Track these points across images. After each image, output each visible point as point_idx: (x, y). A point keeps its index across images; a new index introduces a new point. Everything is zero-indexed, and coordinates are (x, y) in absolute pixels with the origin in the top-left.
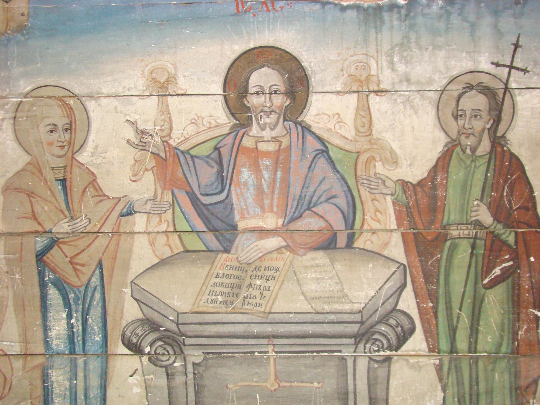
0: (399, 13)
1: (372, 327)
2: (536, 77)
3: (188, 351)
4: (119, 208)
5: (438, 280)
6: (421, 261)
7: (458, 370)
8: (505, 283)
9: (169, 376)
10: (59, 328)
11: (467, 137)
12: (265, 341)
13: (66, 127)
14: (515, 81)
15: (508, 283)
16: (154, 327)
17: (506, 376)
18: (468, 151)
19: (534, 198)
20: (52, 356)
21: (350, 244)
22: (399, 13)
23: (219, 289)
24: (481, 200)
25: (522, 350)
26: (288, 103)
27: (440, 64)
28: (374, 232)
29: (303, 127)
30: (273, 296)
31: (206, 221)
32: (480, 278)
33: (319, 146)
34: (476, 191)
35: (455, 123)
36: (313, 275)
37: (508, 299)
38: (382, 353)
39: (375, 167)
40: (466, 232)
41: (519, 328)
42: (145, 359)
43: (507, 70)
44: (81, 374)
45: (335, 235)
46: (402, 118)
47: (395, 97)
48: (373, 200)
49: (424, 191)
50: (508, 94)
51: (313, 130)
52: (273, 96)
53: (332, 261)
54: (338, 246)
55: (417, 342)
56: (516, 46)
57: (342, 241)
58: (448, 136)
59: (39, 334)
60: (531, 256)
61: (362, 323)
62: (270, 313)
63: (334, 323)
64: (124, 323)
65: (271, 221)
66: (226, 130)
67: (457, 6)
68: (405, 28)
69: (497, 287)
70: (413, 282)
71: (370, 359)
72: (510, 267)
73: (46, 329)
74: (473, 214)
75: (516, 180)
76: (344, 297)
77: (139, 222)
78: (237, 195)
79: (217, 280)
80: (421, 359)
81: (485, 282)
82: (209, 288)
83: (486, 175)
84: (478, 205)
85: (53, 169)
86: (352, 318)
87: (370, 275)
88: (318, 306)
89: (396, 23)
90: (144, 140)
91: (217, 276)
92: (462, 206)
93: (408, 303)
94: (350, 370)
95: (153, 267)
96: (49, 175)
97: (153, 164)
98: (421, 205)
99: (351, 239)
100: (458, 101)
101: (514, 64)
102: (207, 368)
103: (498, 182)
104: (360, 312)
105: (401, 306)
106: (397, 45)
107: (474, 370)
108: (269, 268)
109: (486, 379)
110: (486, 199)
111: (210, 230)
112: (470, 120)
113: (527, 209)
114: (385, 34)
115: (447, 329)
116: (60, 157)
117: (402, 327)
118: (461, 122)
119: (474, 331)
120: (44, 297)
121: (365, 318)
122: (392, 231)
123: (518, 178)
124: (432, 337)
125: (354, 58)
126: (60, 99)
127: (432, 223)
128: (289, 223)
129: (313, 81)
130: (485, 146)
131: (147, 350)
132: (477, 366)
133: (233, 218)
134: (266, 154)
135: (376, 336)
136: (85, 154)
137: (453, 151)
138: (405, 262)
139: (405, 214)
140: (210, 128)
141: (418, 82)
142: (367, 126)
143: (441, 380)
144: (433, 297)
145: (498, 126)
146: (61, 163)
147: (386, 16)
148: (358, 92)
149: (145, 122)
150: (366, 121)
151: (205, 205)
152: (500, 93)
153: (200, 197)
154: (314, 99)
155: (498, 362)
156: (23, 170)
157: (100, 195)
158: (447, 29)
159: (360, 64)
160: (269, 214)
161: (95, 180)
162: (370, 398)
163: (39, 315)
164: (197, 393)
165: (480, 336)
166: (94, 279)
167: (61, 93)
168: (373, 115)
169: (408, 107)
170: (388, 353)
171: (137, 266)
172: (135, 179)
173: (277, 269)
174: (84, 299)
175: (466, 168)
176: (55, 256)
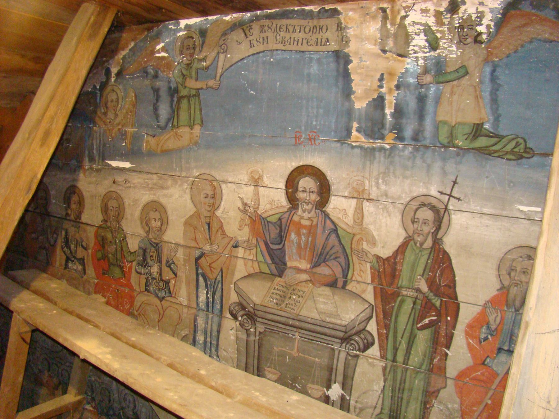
0: (385, 153)
1: (351, 336)
2: (465, 204)
3: (258, 325)
4: (232, 243)
5: (391, 318)
6: (383, 305)
7: (395, 372)
8: (430, 329)
9: (248, 335)
10: (202, 298)
11: (418, 236)
12: (295, 329)
13: (212, 196)
14: (452, 205)
15: (432, 330)
16: (243, 308)
17: (422, 383)
18: (418, 245)
19: (455, 281)
20: (199, 310)
21: (344, 287)
22: (385, 153)
23: (275, 296)
24: (423, 276)
25: (435, 370)
26: (318, 199)
27: (406, 188)
28: (358, 282)
29: (325, 214)
30: (301, 306)
31: (272, 258)
32: (415, 323)
33: (333, 227)
34: (420, 270)
35: (412, 226)
36: (323, 300)
37: (431, 339)
38: (355, 352)
39: (362, 244)
40: (411, 294)
41: (435, 357)
42: (238, 323)
43: (447, 197)
44: (210, 323)
45: (336, 280)
46: (381, 218)
47: (378, 204)
48: (359, 263)
49: (389, 264)
50: (446, 213)
51: (331, 217)
52: (311, 194)
53: (334, 294)
54: (338, 286)
55: (374, 351)
56: (455, 183)
57: (340, 283)
58: (407, 233)
59: (195, 299)
60: (448, 316)
61: (346, 332)
62: (298, 315)
63: (331, 328)
64: (230, 303)
66: (286, 210)
67: (421, 153)
69: (425, 330)
70: (377, 316)
71: (348, 353)
72: (435, 320)
73: (197, 296)
74: (417, 283)
75: (445, 267)
76: (337, 316)
77: (240, 252)
78: (288, 246)
79: (274, 291)
80: (375, 361)
81: (419, 326)
82: (270, 294)
83: (427, 262)
84: (420, 279)
85: (205, 217)
86: (341, 328)
87: (353, 307)
88: (323, 317)
89: (382, 159)
90: (246, 209)
91: (274, 289)
92: (410, 277)
93: (372, 327)
94: (336, 356)
95: (245, 277)
96: (203, 220)
97: (249, 222)
98: (387, 271)
99: (345, 284)
100: (415, 213)
101: (452, 194)
102: (265, 336)
103: (434, 267)
104: (345, 326)
105: (368, 328)
106: (381, 173)
107: (404, 375)
108: (300, 291)
109: (410, 382)
110: (426, 276)
111: (273, 263)
112: (421, 226)
113: (450, 287)
114: (376, 165)
115: (392, 347)
116: (208, 211)
117: (367, 340)
118: (416, 225)
119: (408, 352)
120: (197, 281)
121: (347, 330)
122: (368, 284)
123: (447, 267)
124: (383, 350)
125: (356, 178)
126: (211, 181)
127: (391, 284)
128: (313, 268)
129: (333, 188)
130: (429, 243)
131: (240, 319)
132: (406, 372)
133: (285, 259)
134: (305, 227)
135: (352, 342)
136: (219, 212)
137: (409, 243)
138: (373, 304)
139: (377, 275)
140: (278, 207)
141: (392, 198)
142: (360, 219)
143: (384, 375)
144: (387, 327)
145: (438, 231)
146: (208, 214)
147: (377, 154)
148: (357, 198)
149: (247, 199)
150: (360, 216)
151: (272, 249)
152: (442, 211)
153: (270, 244)
154: (332, 198)
155: (419, 374)
156: (193, 215)
157: (224, 233)
158: (412, 167)
159: (360, 182)
160: (303, 261)
161: (222, 226)
162: (344, 375)
163: (195, 289)
164: (259, 347)
165: (411, 357)
166: (218, 277)
167: (210, 178)
168: (364, 213)
169: (385, 211)
170: (358, 352)
171: (238, 275)
172: (240, 228)
173: (304, 292)
174: (215, 286)
175: (415, 255)
176: (203, 261)
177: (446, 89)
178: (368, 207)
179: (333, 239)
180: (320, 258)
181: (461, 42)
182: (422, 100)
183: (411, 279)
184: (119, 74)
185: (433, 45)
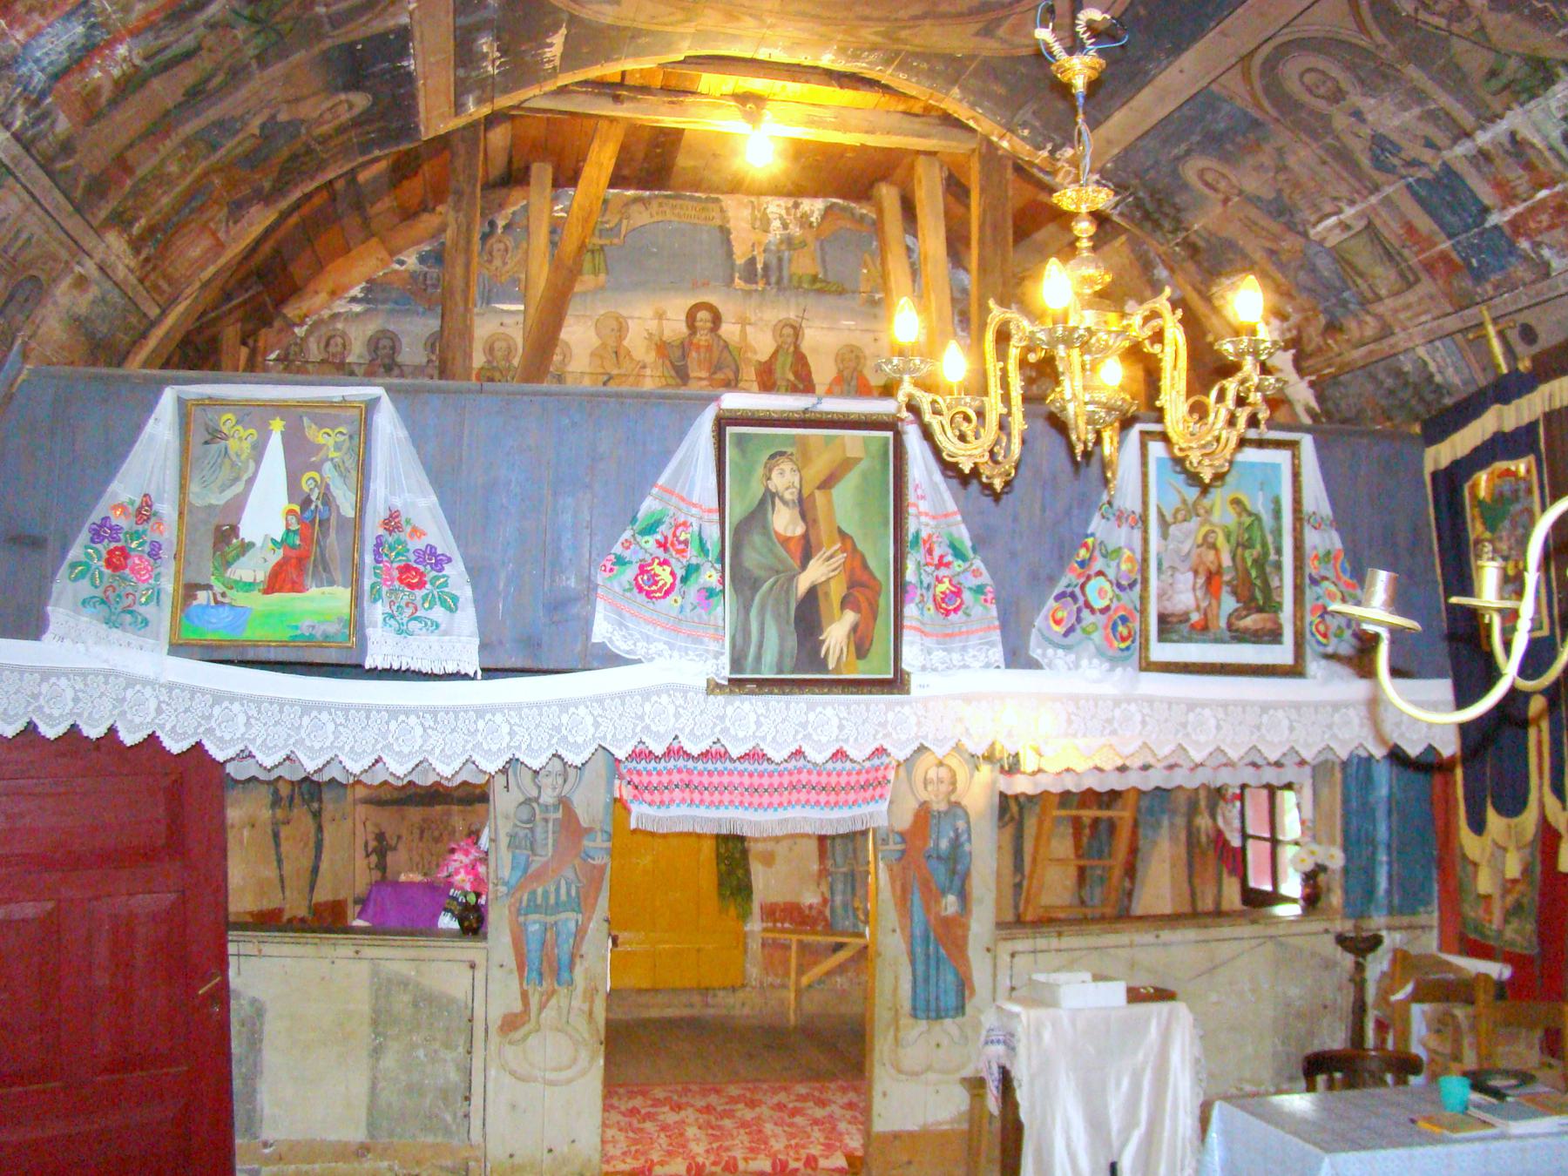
65: (704, 374)
68: (1337, 405)
77: (648, 372)
130: (792, 349)
157: (631, 358)
172: (647, 352)
177: (795, 254)
178: (749, 329)
179: (726, 354)
180: (716, 368)
181: (802, 226)
182: (780, 260)
183: (784, 372)
184: (508, 227)
185: (785, 226)
